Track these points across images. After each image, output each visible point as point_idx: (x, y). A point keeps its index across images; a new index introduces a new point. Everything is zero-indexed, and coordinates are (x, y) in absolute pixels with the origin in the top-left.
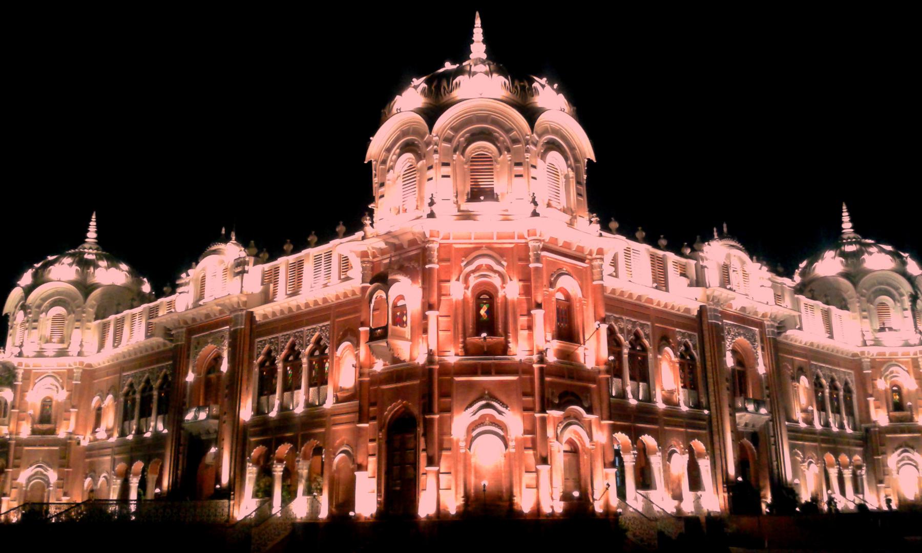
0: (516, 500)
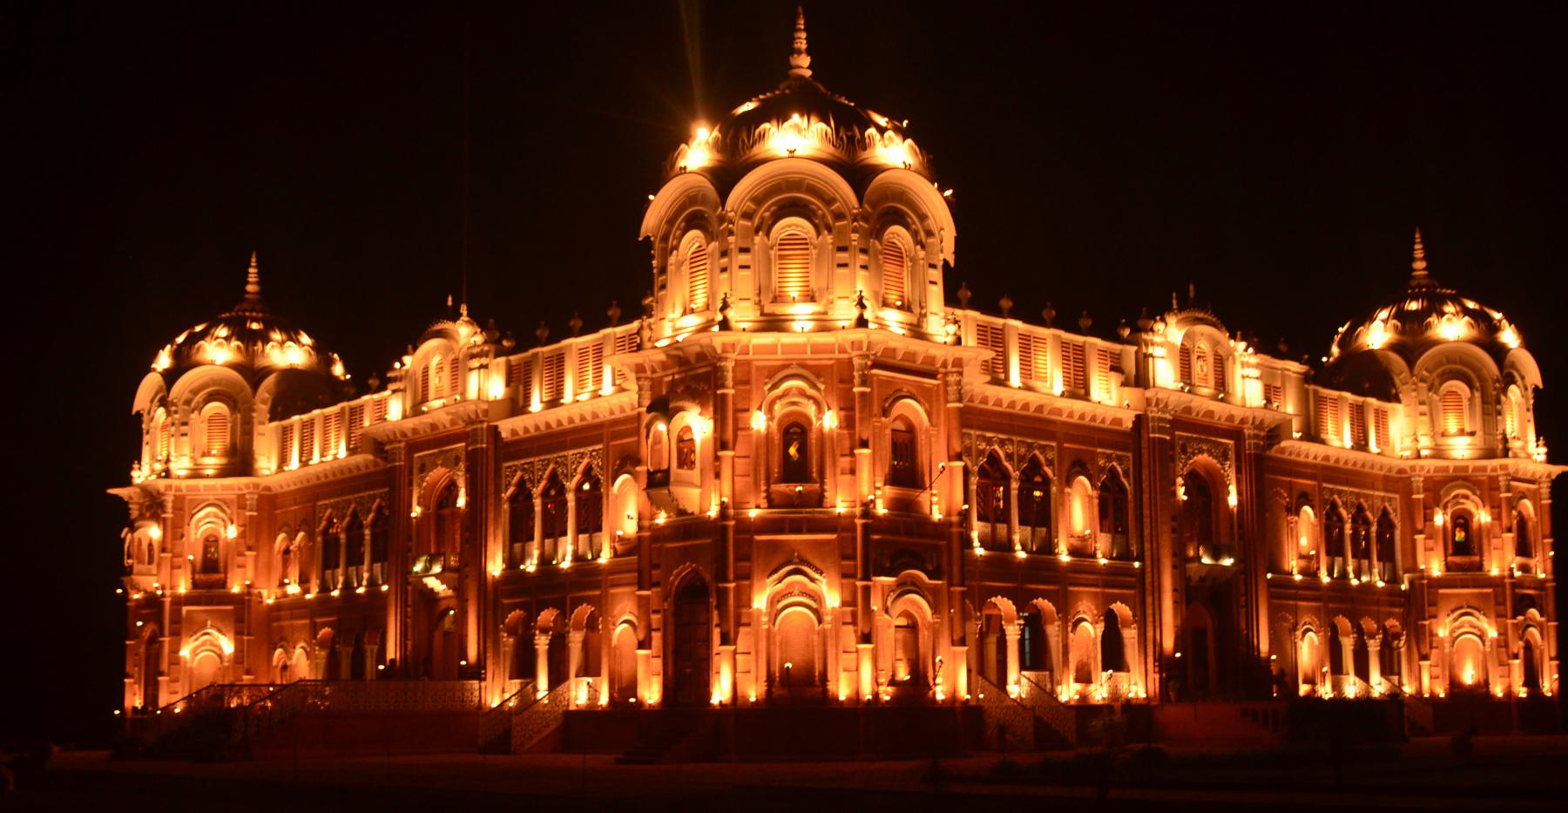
0: (831, 686)
